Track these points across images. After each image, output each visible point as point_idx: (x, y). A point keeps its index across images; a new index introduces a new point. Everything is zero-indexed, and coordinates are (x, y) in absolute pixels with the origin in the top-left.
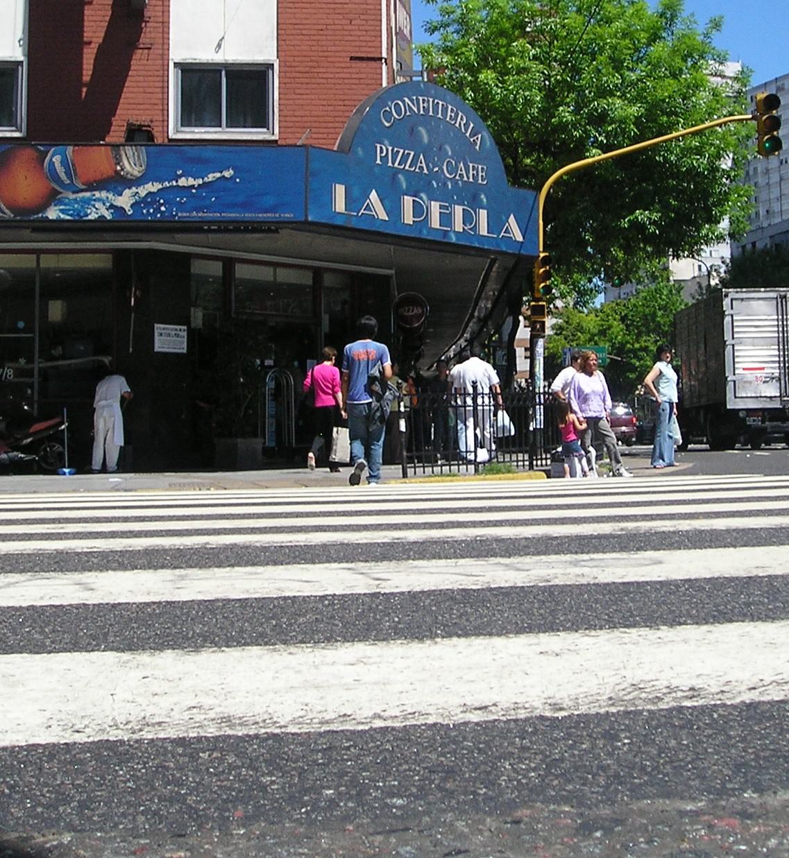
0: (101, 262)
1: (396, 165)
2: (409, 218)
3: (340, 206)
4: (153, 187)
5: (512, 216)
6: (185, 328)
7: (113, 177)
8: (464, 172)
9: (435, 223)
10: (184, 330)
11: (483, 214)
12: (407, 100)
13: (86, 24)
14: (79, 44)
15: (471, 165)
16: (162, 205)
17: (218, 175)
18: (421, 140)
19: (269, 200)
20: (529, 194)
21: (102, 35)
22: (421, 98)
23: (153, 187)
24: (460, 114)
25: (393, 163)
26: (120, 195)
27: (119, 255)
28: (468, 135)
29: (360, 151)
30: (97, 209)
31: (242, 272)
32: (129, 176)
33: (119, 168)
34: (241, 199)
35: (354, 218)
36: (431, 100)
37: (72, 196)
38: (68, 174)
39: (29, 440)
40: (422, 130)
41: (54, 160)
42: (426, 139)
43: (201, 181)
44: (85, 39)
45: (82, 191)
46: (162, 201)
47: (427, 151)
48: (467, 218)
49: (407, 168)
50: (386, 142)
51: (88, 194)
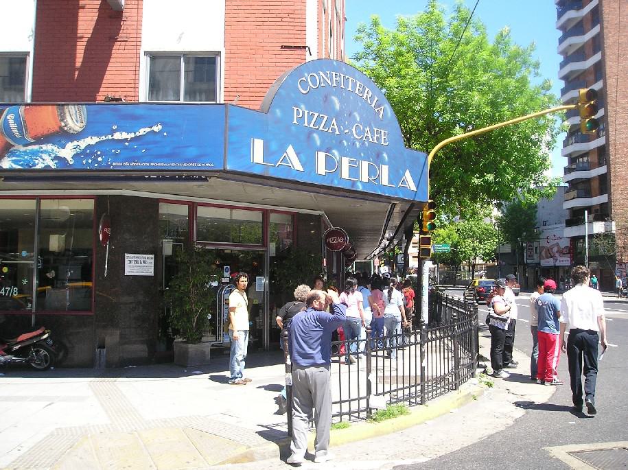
0: (89, 205)
1: (311, 126)
2: (321, 169)
3: (258, 157)
4: (92, 141)
5: (408, 171)
6: (153, 256)
7: (58, 132)
8: (370, 135)
9: (345, 174)
10: (152, 258)
11: (385, 169)
12: (321, 73)
13: (80, 23)
14: (73, 37)
15: (376, 129)
16: (99, 156)
17: (148, 130)
18: (334, 108)
19: (192, 152)
20: (422, 155)
21: (91, 31)
22: (334, 73)
23: (92, 141)
24: (367, 89)
25: (309, 124)
26: (64, 147)
27: (99, 200)
28: (373, 106)
29: (278, 112)
30: (43, 160)
31: (202, 212)
32: (71, 131)
33: (63, 124)
34: (167, 150)
35: (271, 169)
36: (343, 76)
37: (22, 149)
38: (20, 129)
39: (17, 347)
40: (335, 99)
41: (8, 117)
42: (338, 106)
43: (132, 135)
44: (79, 35)
45: (31, 144)
46: (99, 153)
47: (338, 116)
48: (371, 171)
49: (321, 128)
50: (303, 106)
51: (36, 147)
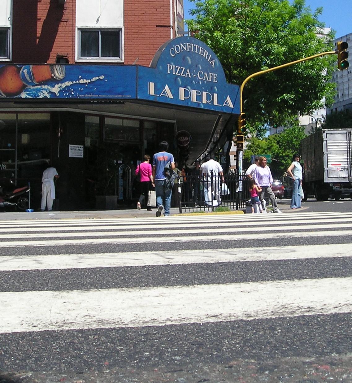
0: (45, 117)
1: (177, 74)
2: (182, 97)
3: (152, 92)
4: (68, 84)
5: (228, 96)
6: (83, 146)
7: (50, 79)
8: (207, 77)
9: (194, 99)
10: (82, 147)
11: (216, 95)
12: (181, 45)
13: (38, 11)
14: (35, 20)
15: (210, 74)
16: (72, 91)
17: (97, 78)
18: (188, 63)
19: (120, 89)
20: (236, 87)
21: (46, 15)
22: (188, 44)
23: (68, 84)
24: (205, 51)
25: (175, 73)
26: (54, 87)
27: (53, 114)
28: (209, 60)
29: (161, 67)
30: (43, 93)
31: (108, 121)
32: (58, 79)
33: (53, 75)
34: (107, 89)
35: (158, 97)
36: (192, 45)
37: (32, 88)
38: (30, 77)
39: (13, 196)
40: (188, 58)
41: (24, 71)
42: (190, 62)
43: (89, 81)
44: (38, 18)
45: (37, 85)
46: (72, 90)
47: (190, 67)
48: (208, 97)
49: (182, 75)
50: (172, 63)
51: (39, 87)
